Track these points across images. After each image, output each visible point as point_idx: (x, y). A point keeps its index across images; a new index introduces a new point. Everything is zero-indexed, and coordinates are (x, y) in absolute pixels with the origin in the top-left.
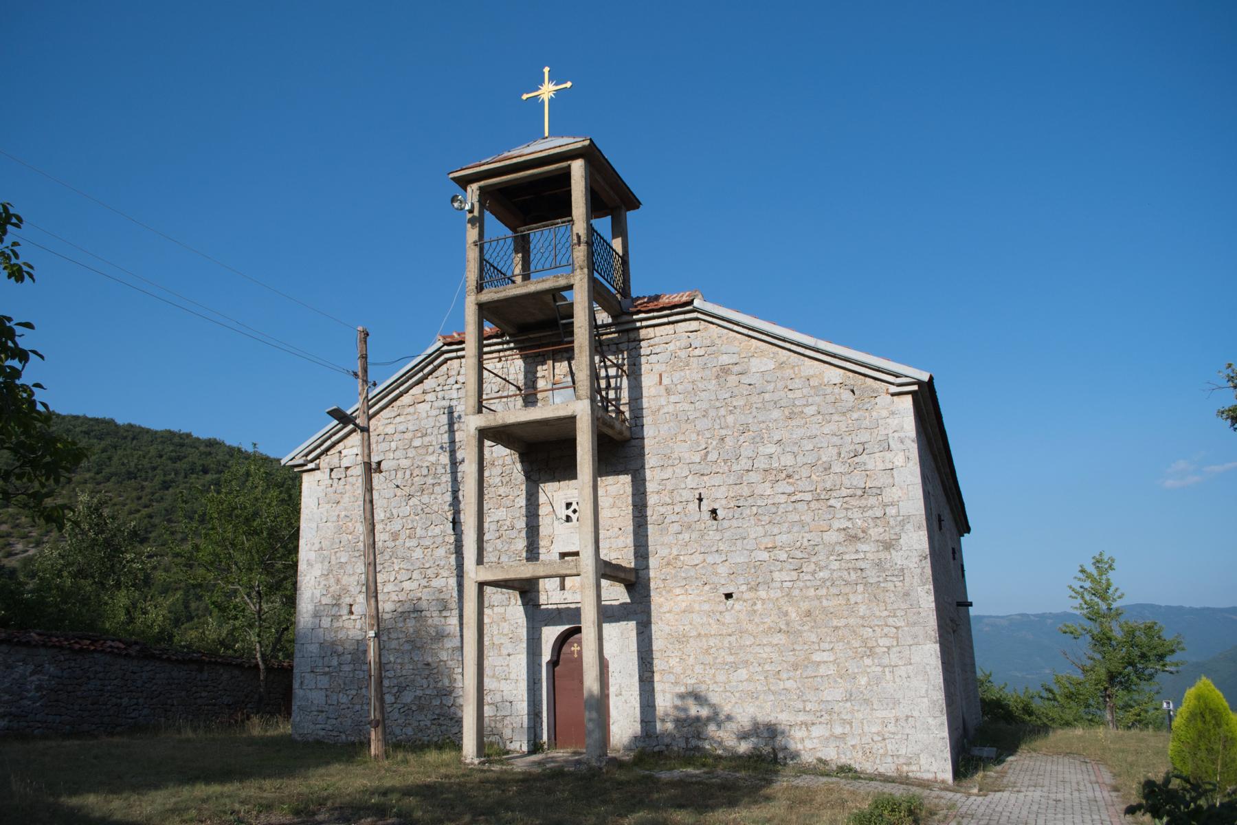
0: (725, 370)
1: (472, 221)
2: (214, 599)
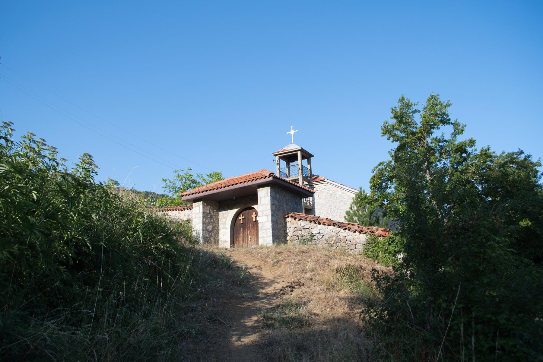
0: (332, 194)
1: (277, 164)
2: (78, 336)
